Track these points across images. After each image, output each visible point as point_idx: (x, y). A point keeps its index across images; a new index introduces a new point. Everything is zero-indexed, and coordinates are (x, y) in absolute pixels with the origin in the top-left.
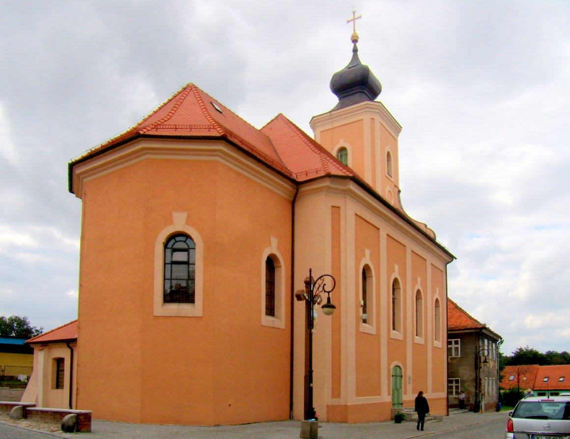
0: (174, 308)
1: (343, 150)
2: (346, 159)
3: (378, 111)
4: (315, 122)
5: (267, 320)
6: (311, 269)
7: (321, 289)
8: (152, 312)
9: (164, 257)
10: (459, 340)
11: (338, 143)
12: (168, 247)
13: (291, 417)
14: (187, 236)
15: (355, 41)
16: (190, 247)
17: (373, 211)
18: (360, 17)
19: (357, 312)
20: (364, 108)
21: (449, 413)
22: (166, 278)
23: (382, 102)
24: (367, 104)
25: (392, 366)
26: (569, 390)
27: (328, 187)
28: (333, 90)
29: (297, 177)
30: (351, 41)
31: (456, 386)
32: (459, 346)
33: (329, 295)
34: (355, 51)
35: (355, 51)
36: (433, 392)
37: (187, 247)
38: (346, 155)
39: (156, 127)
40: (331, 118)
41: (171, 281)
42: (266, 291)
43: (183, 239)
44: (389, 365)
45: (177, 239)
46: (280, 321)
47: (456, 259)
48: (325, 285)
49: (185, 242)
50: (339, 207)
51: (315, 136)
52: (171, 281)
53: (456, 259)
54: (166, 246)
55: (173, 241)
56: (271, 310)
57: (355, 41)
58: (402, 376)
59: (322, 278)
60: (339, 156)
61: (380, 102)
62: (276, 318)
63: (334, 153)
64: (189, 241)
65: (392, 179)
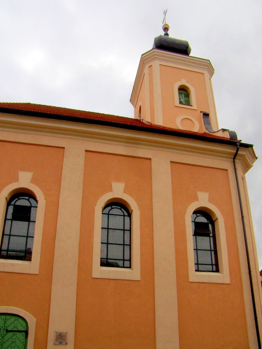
3: (207, 68)
8: (188, 280)
9: (246, 237)
14: (31, 195)
15: (165, 13)
16: (33, 205)
17: (173, 149)
22: (5, 233)
23: (210, 61)
24: (154, 51)
26: (260, 347)
37: (29, 205)
41: (9, 238)
42: (228, 249)
49: (28, 200)
52: (9, 238)
57: (165, 13)
58: (26, 332)
61: (209, 61)
64: (32, 200)
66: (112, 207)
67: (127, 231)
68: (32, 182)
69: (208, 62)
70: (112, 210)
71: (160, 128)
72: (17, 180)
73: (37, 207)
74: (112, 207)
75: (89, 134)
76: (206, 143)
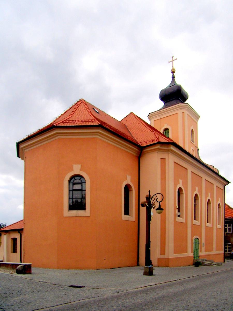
0: (74, 213)
1: (166, 129)
2: (168, 134)
4: (150, 116)
5: (125, 217)
6: (149, 191)
7: (155, 201)
10: (231, 224)
11: (164, 126)
12: (71, 182)
13: (138, 264)
14: (81, 177)
15: (173, 72)
18: (176, 59)
19: (175, 212)
20: (179, 107)
21: (225, 261)
25: (194, 238)
27: (159, 149)
28: (161, 99)
29: (141, 145)
30: (171, 72)
31: (229, 247)
32: (231, 227)
33: (160, 203)
34: (173, 77)
35: (173, 77)
36: (216, 250)
38: (168, 132)
39: (63, 122)
40: (160, 114)
43: (79, 178)
44: (192, 237)
45: (76, 178)
46: (132, 217)
47: (230, 183)
48: (157, 198)
49: (80, 179)
50: (165, 159)
51: (151, 123)
53: (230, 183)
54: (69, 182)
55: (73, 179)
56: (127, 212)
57: (173, 72)
59: (156, 195)
60: (164, 133)
61: (188, 104)
62: (130, 216)
63: (162, 131)
64: (82, 179)
65: (194, 144)
66: (75, 179)
67: (71, 190)
68: (81, 170)
69: (188, 105)
70: (79, 180)
71: (128, 137)
72: (72, 170)
73: (85, 183)
74: (75, 179)
75: (182, 157)
76: (180, 151)
